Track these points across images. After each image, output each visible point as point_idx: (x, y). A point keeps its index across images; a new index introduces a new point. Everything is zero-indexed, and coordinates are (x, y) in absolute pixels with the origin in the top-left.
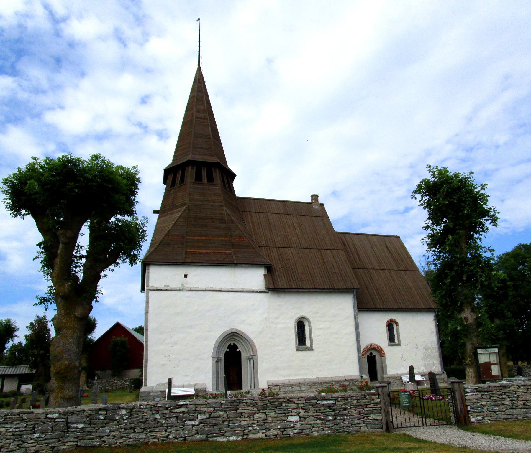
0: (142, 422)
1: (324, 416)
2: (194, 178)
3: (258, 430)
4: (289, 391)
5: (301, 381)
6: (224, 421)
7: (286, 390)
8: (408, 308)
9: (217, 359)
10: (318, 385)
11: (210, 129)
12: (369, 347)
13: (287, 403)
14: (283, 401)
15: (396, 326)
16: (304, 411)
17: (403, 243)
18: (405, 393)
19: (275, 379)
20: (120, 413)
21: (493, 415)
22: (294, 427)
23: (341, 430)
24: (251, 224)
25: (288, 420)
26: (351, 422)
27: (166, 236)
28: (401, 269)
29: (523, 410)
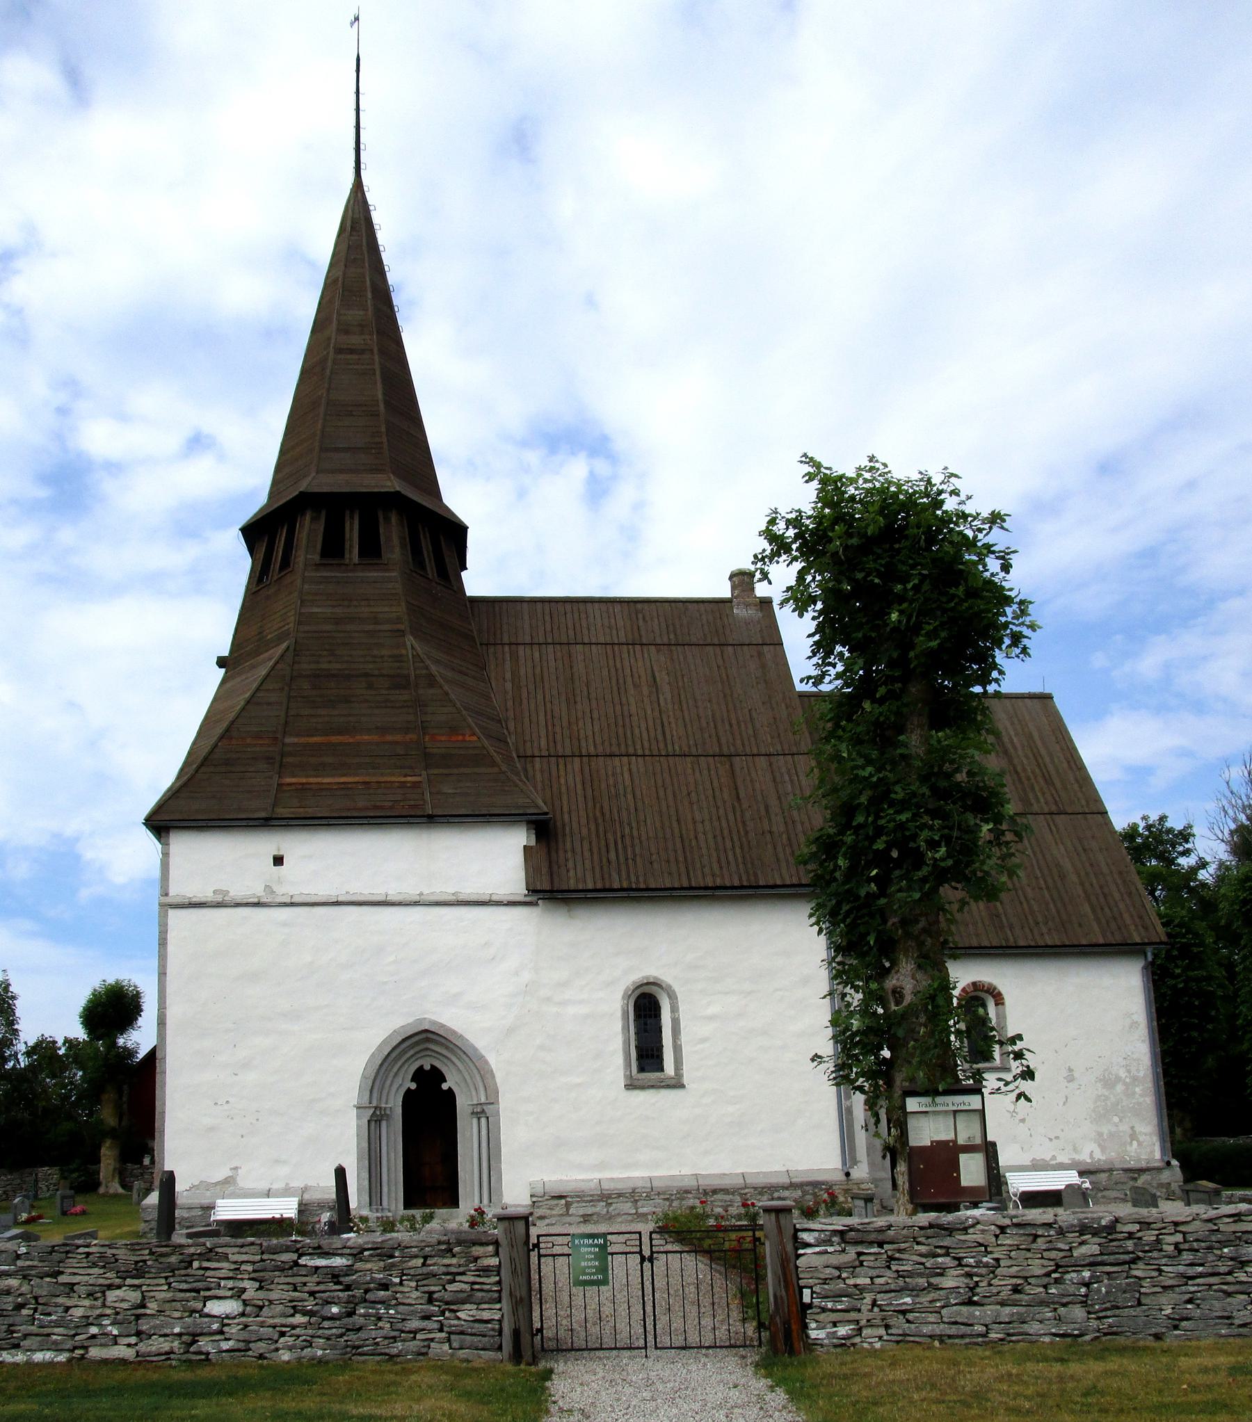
1: (316, 1304)
2: (319, 546)
3: (116, 1336)
4: (598, 1214)
5: (640, 1184)
6: (19, 1307)
7: (590, 1211)
8: (1041, 943)
9: (372, 1111)
10: (695, 1198)
11: (379, 385)
13: (208, 1260)
14: (193, 1254)
15: (996, 1005)
16: (257, 1285)
17: (1061, 720)
18: (591, 1241)
19: (554, 1178)
21: (892, 1322)
22: (221, 1332)
23: (365, 1349)
24: (509, 685)
25: (206, 1310)
26: (399, 1326)
27: (221, 738)
28: (1036, 808)
29: (1007, 1310)
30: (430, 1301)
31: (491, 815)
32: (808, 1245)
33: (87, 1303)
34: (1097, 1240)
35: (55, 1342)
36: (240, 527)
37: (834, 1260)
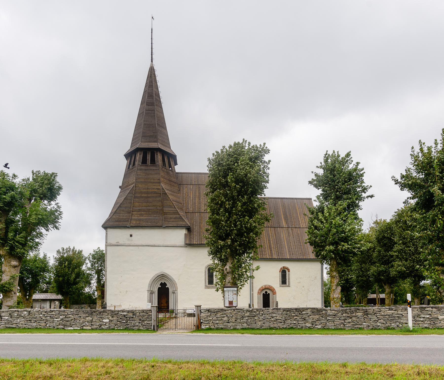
0: (34, 318)
2: (141, 162)
12: (264, 287)
19: (189, 307)
20: (24, 313)
30: (140, 320)
31: (177, 226)
32: (202, 312)
33: (83, 319)
34: (249, 313)
35: (78, 326)
36: (124, 154)
37: (206, 315)
